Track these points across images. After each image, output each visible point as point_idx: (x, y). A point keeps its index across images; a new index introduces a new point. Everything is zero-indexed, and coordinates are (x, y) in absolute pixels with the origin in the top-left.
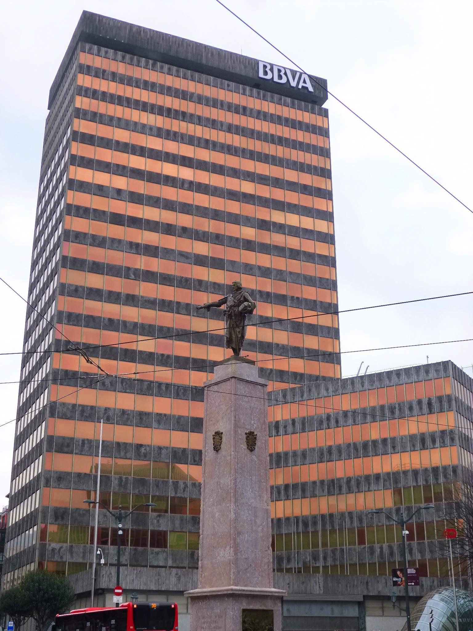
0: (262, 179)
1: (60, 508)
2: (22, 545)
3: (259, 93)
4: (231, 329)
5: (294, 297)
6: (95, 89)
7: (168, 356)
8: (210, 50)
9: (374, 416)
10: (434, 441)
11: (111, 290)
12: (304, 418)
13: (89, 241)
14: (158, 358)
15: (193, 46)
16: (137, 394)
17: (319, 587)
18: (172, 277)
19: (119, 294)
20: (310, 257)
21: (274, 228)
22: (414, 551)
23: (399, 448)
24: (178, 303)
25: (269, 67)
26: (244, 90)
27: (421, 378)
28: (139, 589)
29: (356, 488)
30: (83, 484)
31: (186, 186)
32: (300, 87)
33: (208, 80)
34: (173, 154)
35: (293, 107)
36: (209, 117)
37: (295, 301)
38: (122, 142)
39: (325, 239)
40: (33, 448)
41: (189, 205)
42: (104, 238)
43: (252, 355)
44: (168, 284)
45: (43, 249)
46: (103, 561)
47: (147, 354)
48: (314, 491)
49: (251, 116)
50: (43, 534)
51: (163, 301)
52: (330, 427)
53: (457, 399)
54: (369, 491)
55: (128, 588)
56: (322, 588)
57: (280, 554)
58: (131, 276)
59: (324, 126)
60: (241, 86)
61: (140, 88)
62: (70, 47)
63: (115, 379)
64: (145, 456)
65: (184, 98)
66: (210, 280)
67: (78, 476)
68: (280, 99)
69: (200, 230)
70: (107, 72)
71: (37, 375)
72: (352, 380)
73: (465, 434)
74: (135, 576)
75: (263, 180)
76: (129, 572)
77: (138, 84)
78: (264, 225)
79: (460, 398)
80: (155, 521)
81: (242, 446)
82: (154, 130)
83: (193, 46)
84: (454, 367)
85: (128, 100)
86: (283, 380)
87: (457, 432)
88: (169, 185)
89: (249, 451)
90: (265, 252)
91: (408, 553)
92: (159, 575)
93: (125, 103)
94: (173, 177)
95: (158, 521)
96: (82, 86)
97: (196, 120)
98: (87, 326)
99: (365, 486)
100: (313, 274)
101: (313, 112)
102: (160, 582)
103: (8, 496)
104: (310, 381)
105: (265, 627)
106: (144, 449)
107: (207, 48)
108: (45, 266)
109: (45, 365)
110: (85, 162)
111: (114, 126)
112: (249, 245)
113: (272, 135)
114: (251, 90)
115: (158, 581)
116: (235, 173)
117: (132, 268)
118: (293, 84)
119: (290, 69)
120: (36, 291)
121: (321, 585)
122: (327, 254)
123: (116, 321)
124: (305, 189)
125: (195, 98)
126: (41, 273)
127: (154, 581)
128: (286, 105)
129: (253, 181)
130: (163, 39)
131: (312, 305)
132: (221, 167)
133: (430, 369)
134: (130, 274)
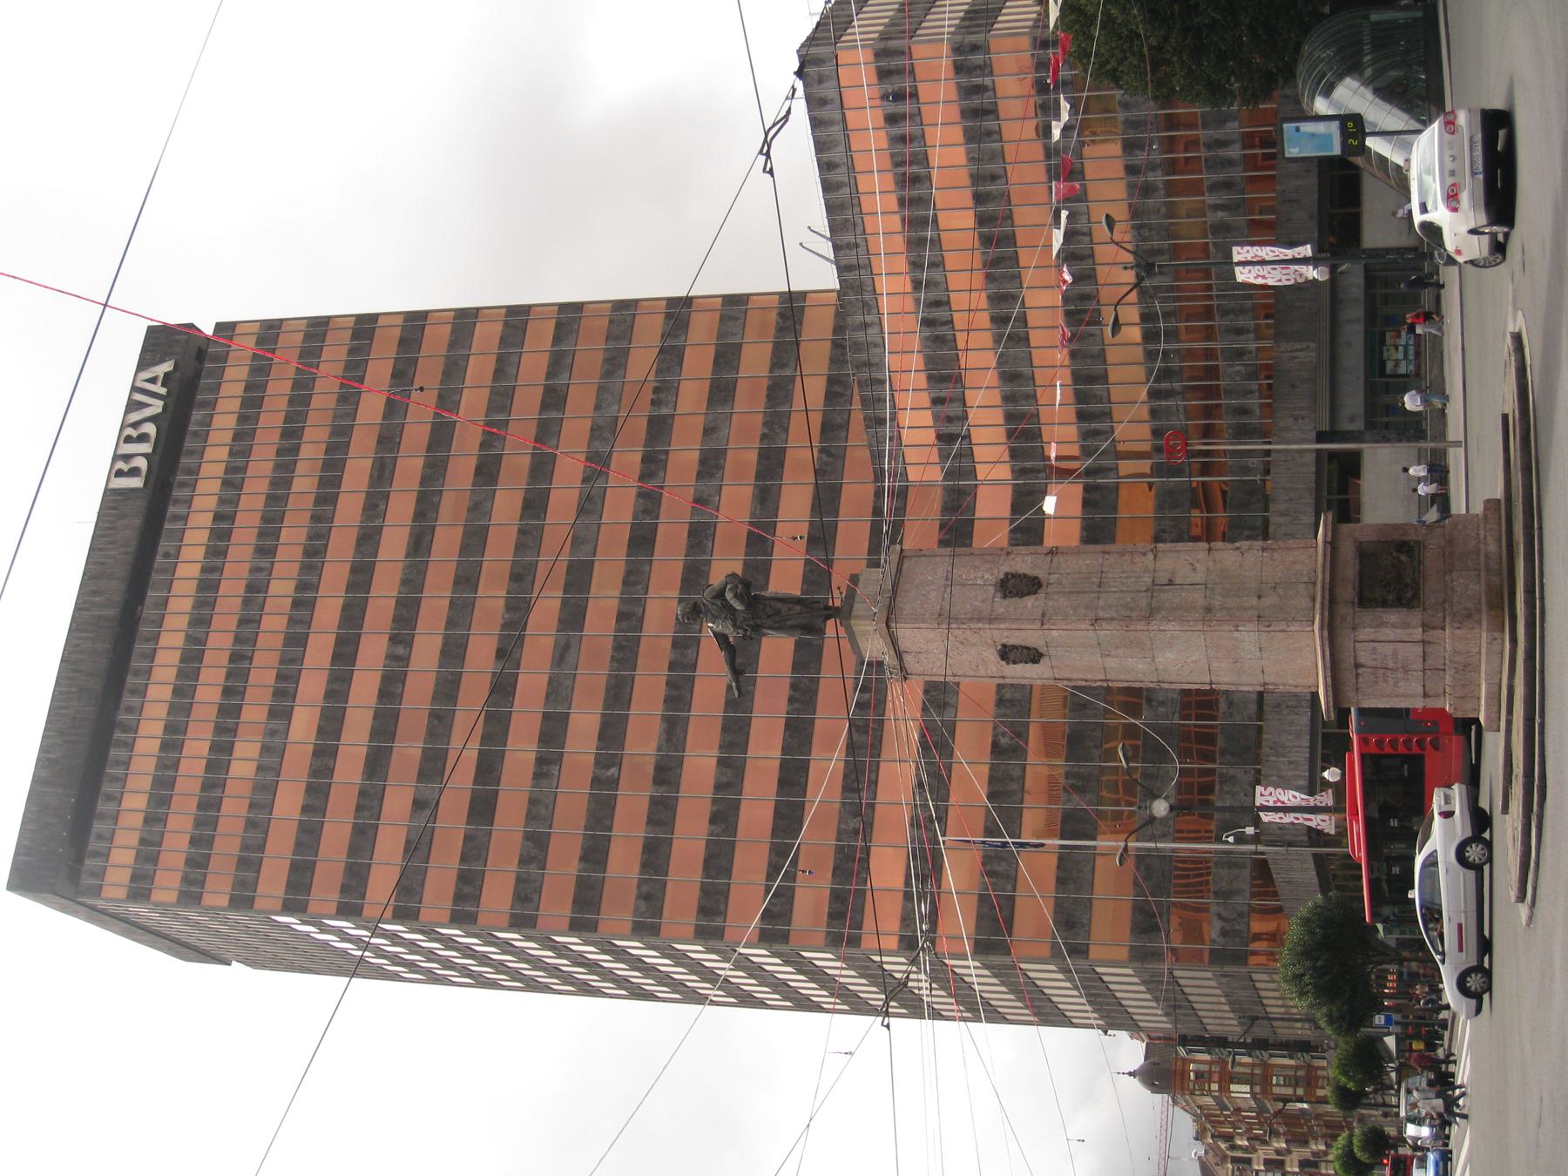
0: (380, 477)
1: (1134, 922)
2: (1214, 999)
3: (183, 485)
4: (781, 626)
5: (652, 400)
6: (186, 864)
7: (794, 687)
8: (86, 598)
9: (923, 222)
10: (979, 89)
11: (646, 819)
12: (929, 378)
13: (533, 870)
14: (798, 711)
15: (80, 639)
16: (879, 756)
17: (1301, 350)
18: (613, 681)
19: (654, 802)
20: (559, 362)
21: (493, 446)
22: (1221, 137)
23: (994, 167)
24: (673, 666)
25: (121, 465)
26: (176, 518)
27: (837, 115)
28: (1308, 750)
29: (1084, 262)
30: (1082, 872)
31: (401, 651)
32: (163, 391)
33: (156, 604)
34: (328, 682)
35: (212, 404)
36: (241, 599)
37: (662, 396)
38: (305, 799)
39: (517, 328)
40: (1003, 984)
41: (445, 645)
42: (528, 837)
43: (839, 580)
44: (629, 690)
45: (554, 971)
46: (1250, 830)
47: (790, 736)
48: (1093, 356)
49: (235, 501)
50: (1193, 959)
51: (668, 700)
52: (949, 319)
53: (884, 37)
54: (1090, 234)
55: (1307, 774)
56: (1304, 345)
57: (1230, 431)
58: (613, 775)
59: (257, 331)
60: (167, 526)
61: (179, 759)
62: (89, 919)
63: (848, 807)
64: (1021, 733)
65: (199, 656)
66: (617, 593)
67: (1063, 884)
68: (195, 434)
69: (503, 619)
70: (145, 835)
71: (829, 971)
72: (842, 269)
73: (963, 19)
74: (1281, 759)
75: (383, 472)
76: (1272, 772)
77: (170, 764)
78: (487, 471)
79: (881, 28)
80: (1162, 710)
81: (1029, 605)
82: (275, 727)
83: (80, 639)
84: (811, 41)
85: (208, 786)
86: (843, 422)
87: (959, 38)
88: (400, 691)
89: (1042, 591)
90: (551, 467)
91: (1225, 149)
92: (1278, 706)
93: (216, 793)
94: (382, 682)
95: (1162, 703)
96: (180, 891)
97: (249, 629)
98: (728, 872)
99: (1079, 242)
100: (600, 356)
101: (223, 358)
102: (1294, 703)
103: (1106, 1032)
104: (845, 362)
105: (1394, 558)
106: (1002, 739)
107: (82, 606)
108: (592, 967)
109: (818, 963)
110: (354, 883)
111: (270, 819)
112: (535, 504)
113: (279, 452)
114: (177, 502)
115: (1293, 707)
116: (369, 538)
117: (594, 773)
118: (157, 406)
119: (126, 413)
120: (648, 984)
121: (1298, 346)
122: (552, 324)
123: (715, 808)
124: (403, 374)
125: (199, 631)
126: (607, 975)
127: (1290, 718)
128: (208, 420)
129: (387, 496)
130: (65, 708)
131: (671, 357)
132: (355, 570)
133: (818, 96)
134: (608, 778)
